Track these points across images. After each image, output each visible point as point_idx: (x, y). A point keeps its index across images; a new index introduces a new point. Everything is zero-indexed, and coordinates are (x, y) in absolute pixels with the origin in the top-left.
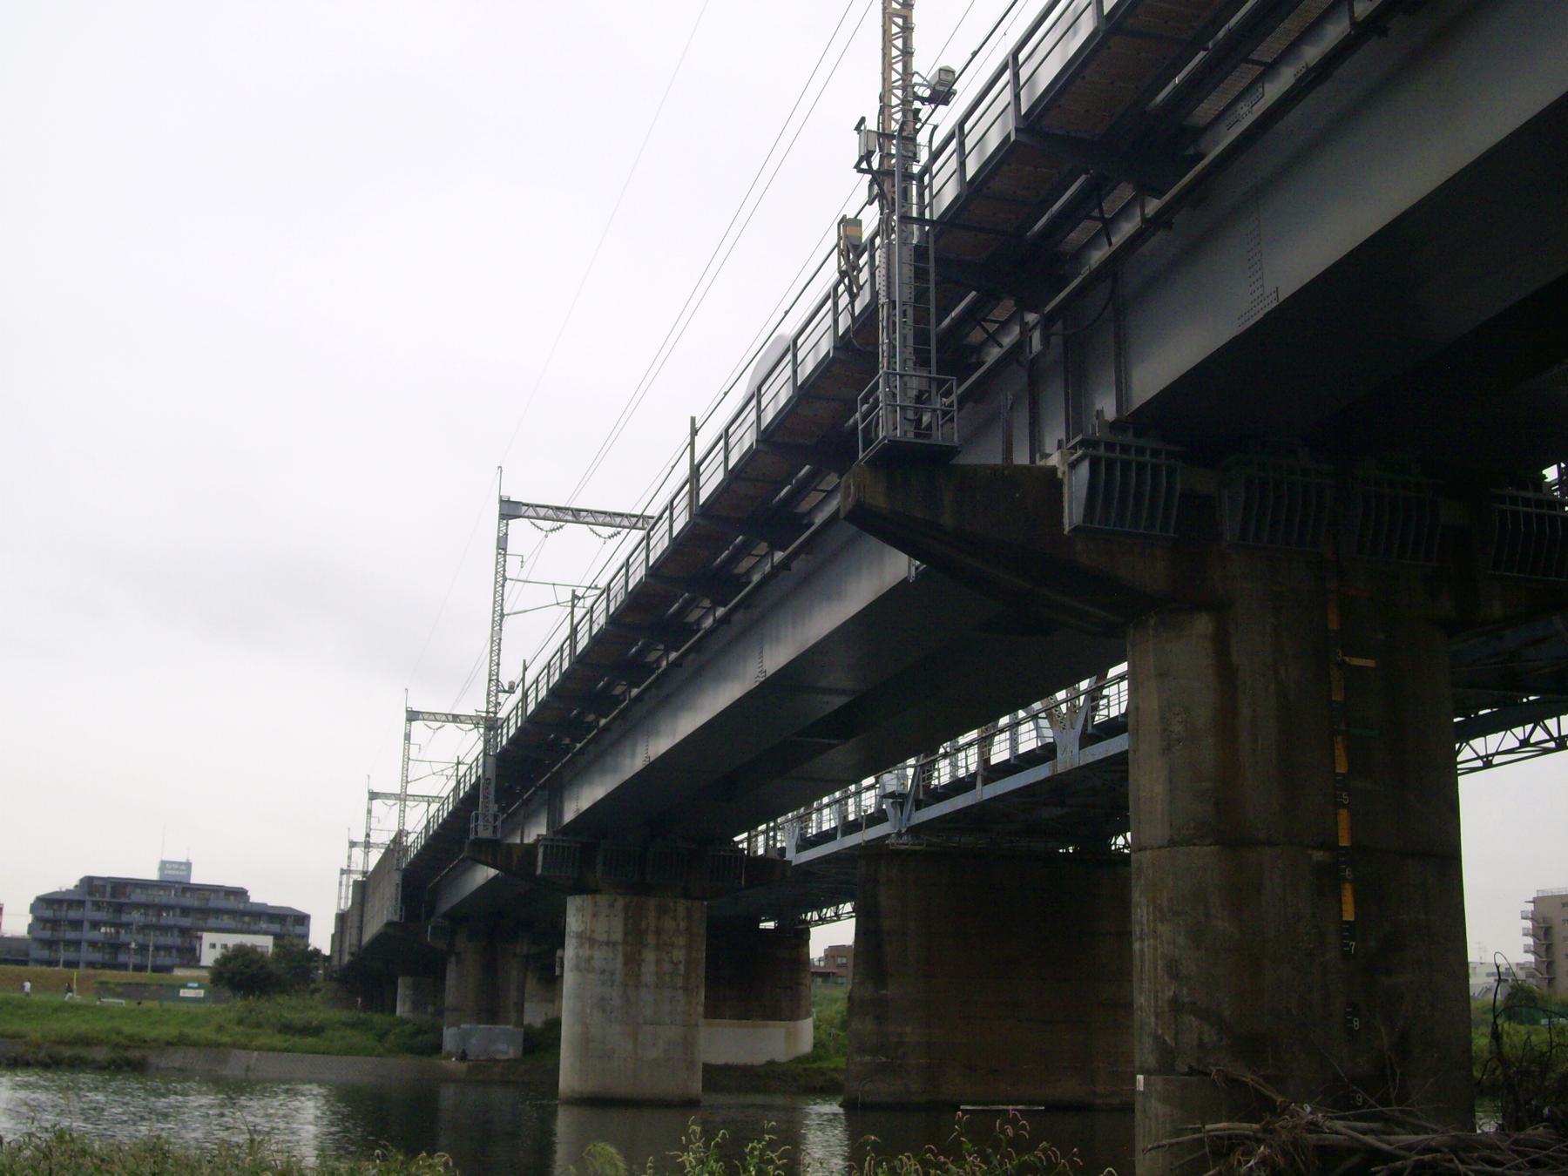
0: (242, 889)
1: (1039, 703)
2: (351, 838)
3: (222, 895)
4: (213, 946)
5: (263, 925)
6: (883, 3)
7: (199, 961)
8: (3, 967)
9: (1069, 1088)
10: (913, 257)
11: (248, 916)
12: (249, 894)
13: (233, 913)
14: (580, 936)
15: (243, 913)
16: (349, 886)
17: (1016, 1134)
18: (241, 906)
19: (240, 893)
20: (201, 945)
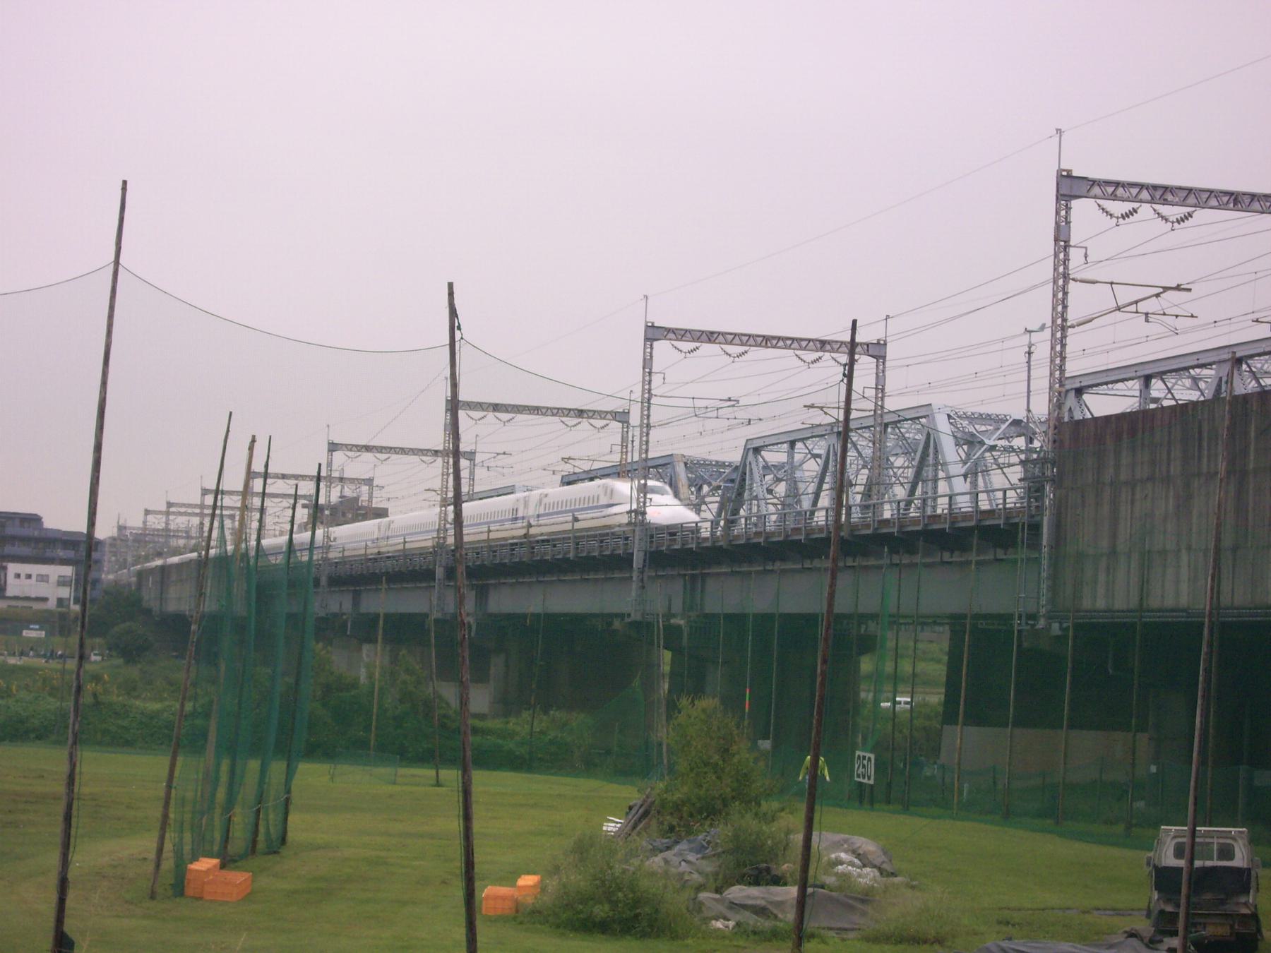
0: (36, 515)
1: (1151, 408)
2: (330, 438)
3: (17, 522)
4: (18, 576)
5: (61, 553)
6: (1266, 196)
7: (4, 590)
8: (1268, 349)
9: (311, 584)
10: (835, 501)
11: (1214, 364)
12: (43, 520)
13: (26, 540)
14: (381, 522)
15: (38, 540)
16: (448, 475)
17: (38, 674)
18: (36, 533)
19: (34, 520)
20: (6, 574)
